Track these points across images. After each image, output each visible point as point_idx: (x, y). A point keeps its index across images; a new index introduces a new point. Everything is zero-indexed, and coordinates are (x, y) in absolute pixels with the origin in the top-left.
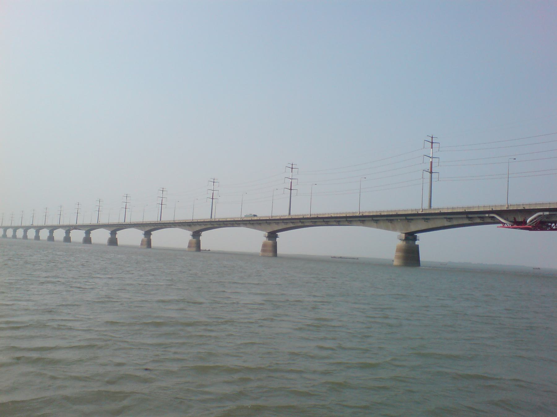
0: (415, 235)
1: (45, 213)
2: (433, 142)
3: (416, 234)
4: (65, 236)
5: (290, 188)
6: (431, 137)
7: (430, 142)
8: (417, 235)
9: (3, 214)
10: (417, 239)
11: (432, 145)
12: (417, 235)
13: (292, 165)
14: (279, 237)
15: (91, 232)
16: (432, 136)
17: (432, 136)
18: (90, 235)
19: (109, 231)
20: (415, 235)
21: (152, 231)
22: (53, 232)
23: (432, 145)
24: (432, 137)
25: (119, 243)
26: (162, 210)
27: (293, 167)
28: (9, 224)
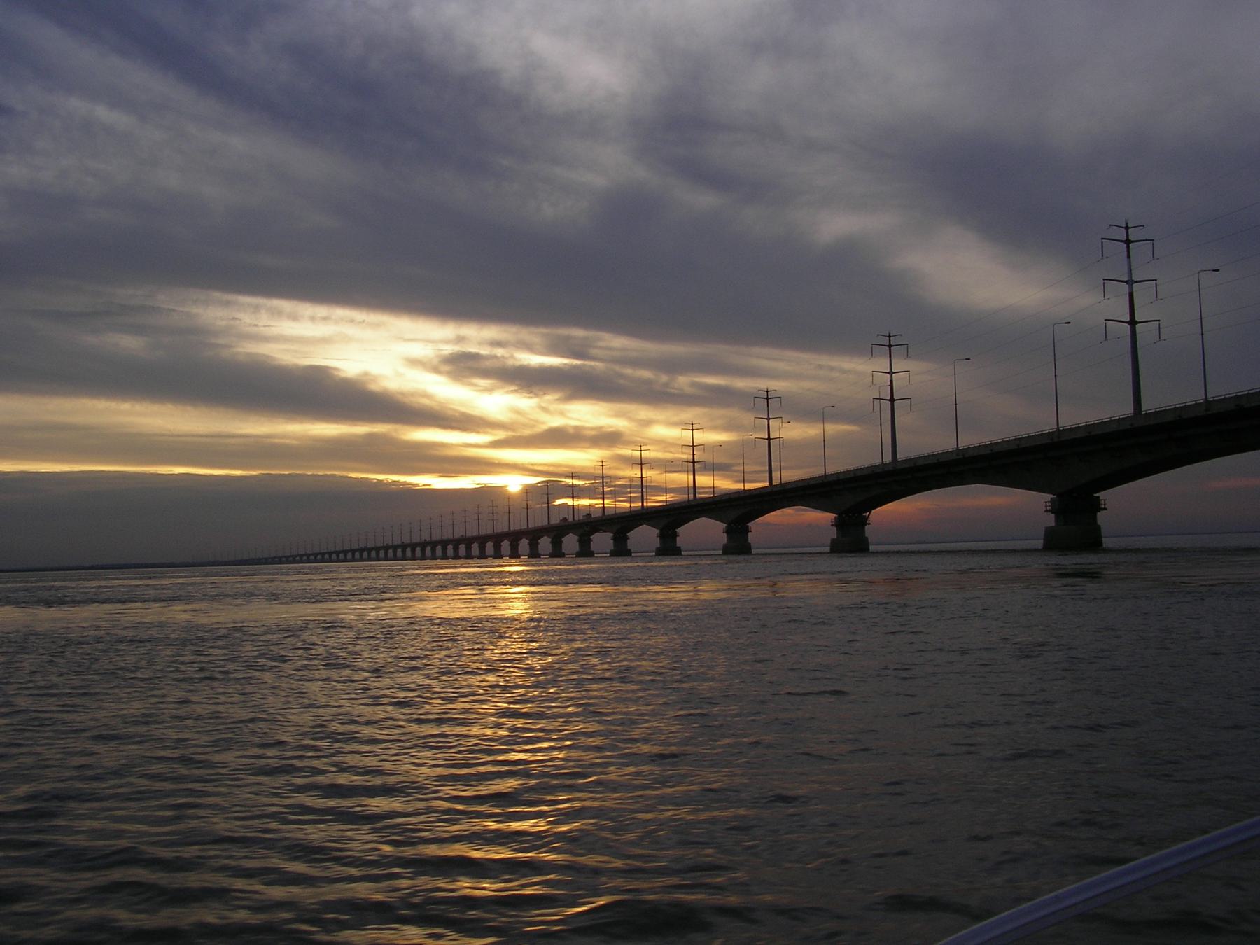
0: (1095, 495)
1: (546, 496)
2: (1131, 238)
3: (1097, 495)
4: (658, 546)
5: (889, 398)
6: (1124, 226)
7: (1122, 241)
8: (1099, 497)
9: (411, 524)
11: (1128, 248)
12: (1099, 497)
13: (890, 337)
14: (1105, 509)
15: (678, 530)
16: (1127, 224)
17: (1127, 224)
18: (628, 545)
19: (657, 529)
20: (1095, 495)
21: (750, 521)
22: (561, 542)
23: (1128, 248)
24: (1127, 228)
25: (1107, 542)
26: (1059, 407)
27: (892, 343)
28: (333, 550)
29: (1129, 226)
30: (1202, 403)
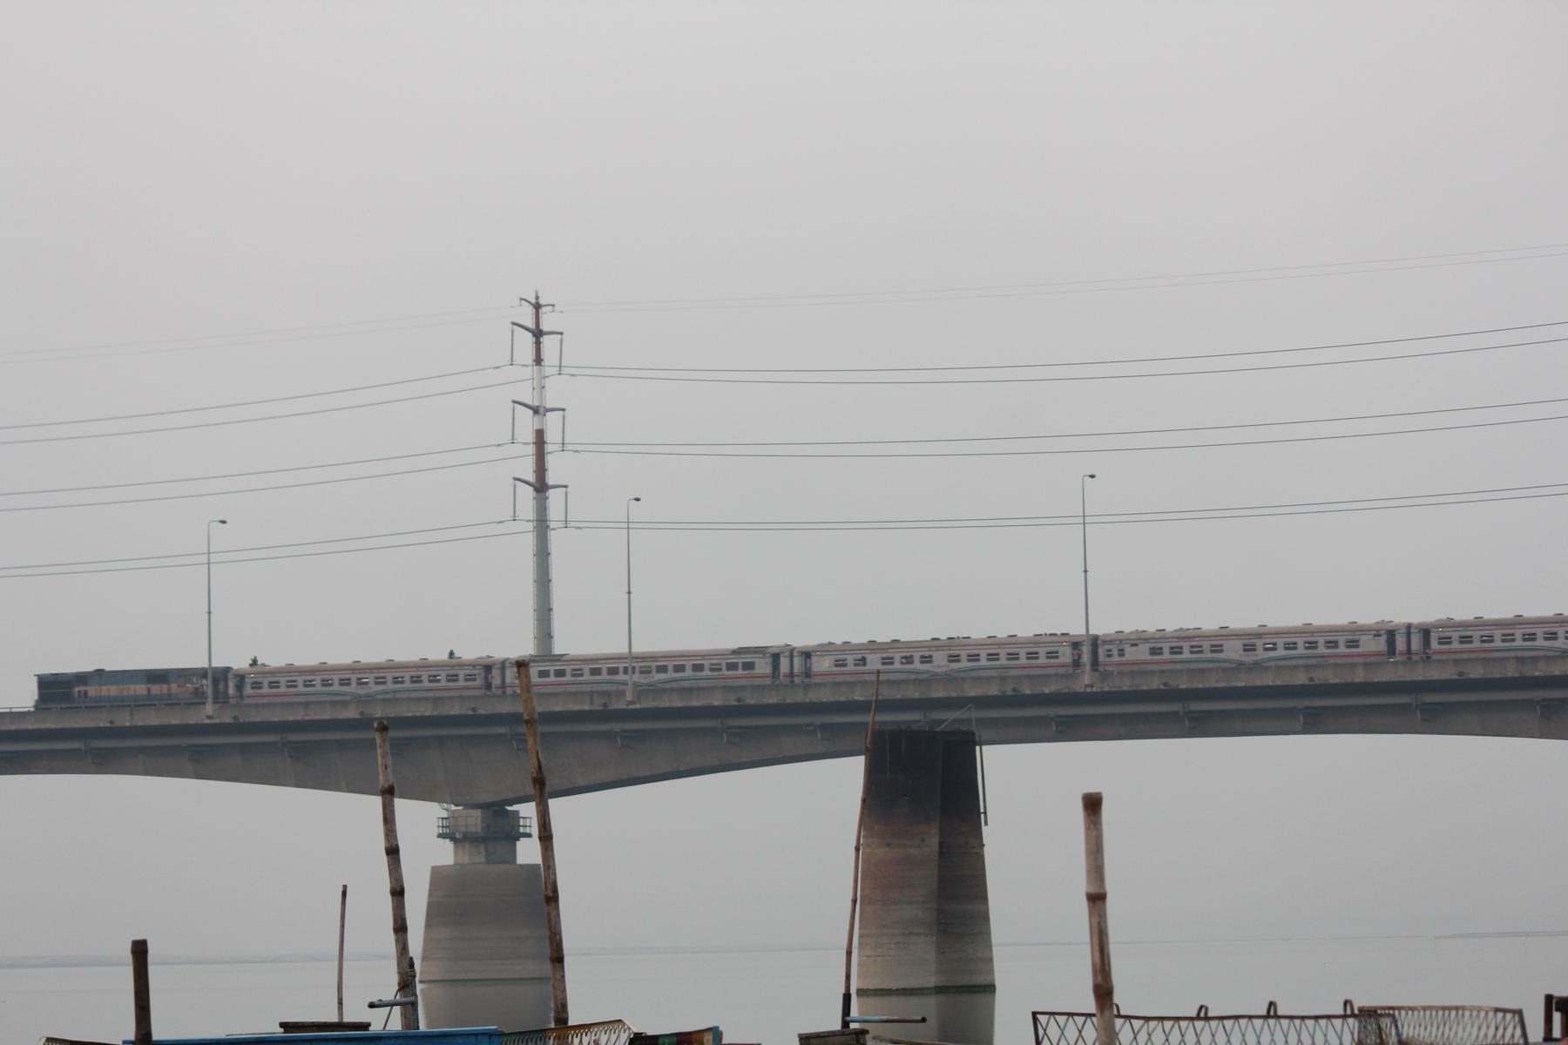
10: (522, 830)
12: (517, 812)
16: (537, 298)
24: (537, 307)
29: (542, 302)
30: (1112, 672)
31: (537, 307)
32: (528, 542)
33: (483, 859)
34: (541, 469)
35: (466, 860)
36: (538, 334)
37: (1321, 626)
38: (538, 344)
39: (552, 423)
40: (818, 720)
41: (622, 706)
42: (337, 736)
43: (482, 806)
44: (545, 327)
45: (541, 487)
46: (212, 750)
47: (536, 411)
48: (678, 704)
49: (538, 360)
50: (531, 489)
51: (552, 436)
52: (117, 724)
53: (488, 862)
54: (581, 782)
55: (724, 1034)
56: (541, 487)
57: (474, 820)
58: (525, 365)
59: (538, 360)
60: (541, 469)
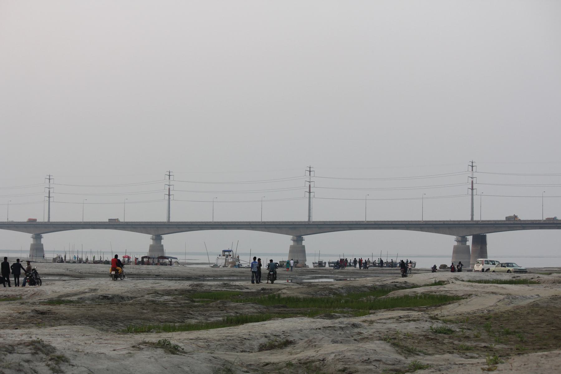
24: (472, 162)
31: (472, 162)
32: (470, 197)
33: (461, 244)
34: (472, 186)
35: (459, 244)
36: (472, 166)
37: (274, 222)
38: (472, 168)
39: (474, 180)
40: (507, 226)
41: (479, 223)
42: (485, 226)
43: (297, 236)
44: (473, 165)
45: (472, 189)
46: (423, 227)
47: (472, 178)
48: (487, 223)
49: (472, 170)
50: (471, 190)
51: (474, 182)
52: (409, 223)
53: (462, 245)
54: (309, 233)
55: (44, 245)
56: (472, 189)
57: (460, 239)
58: (8, 219)
59: (472, 170)
60: (472, 186)
